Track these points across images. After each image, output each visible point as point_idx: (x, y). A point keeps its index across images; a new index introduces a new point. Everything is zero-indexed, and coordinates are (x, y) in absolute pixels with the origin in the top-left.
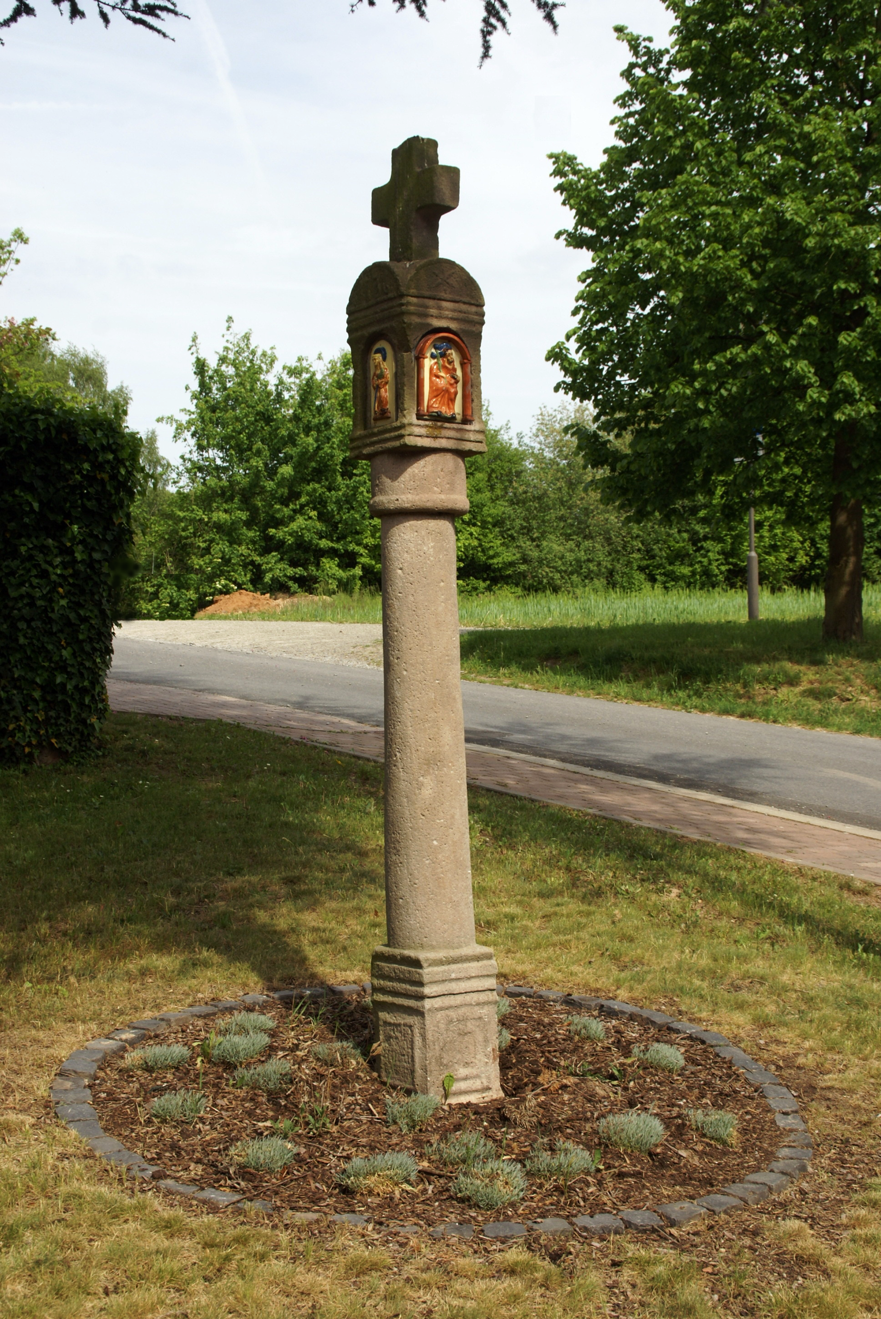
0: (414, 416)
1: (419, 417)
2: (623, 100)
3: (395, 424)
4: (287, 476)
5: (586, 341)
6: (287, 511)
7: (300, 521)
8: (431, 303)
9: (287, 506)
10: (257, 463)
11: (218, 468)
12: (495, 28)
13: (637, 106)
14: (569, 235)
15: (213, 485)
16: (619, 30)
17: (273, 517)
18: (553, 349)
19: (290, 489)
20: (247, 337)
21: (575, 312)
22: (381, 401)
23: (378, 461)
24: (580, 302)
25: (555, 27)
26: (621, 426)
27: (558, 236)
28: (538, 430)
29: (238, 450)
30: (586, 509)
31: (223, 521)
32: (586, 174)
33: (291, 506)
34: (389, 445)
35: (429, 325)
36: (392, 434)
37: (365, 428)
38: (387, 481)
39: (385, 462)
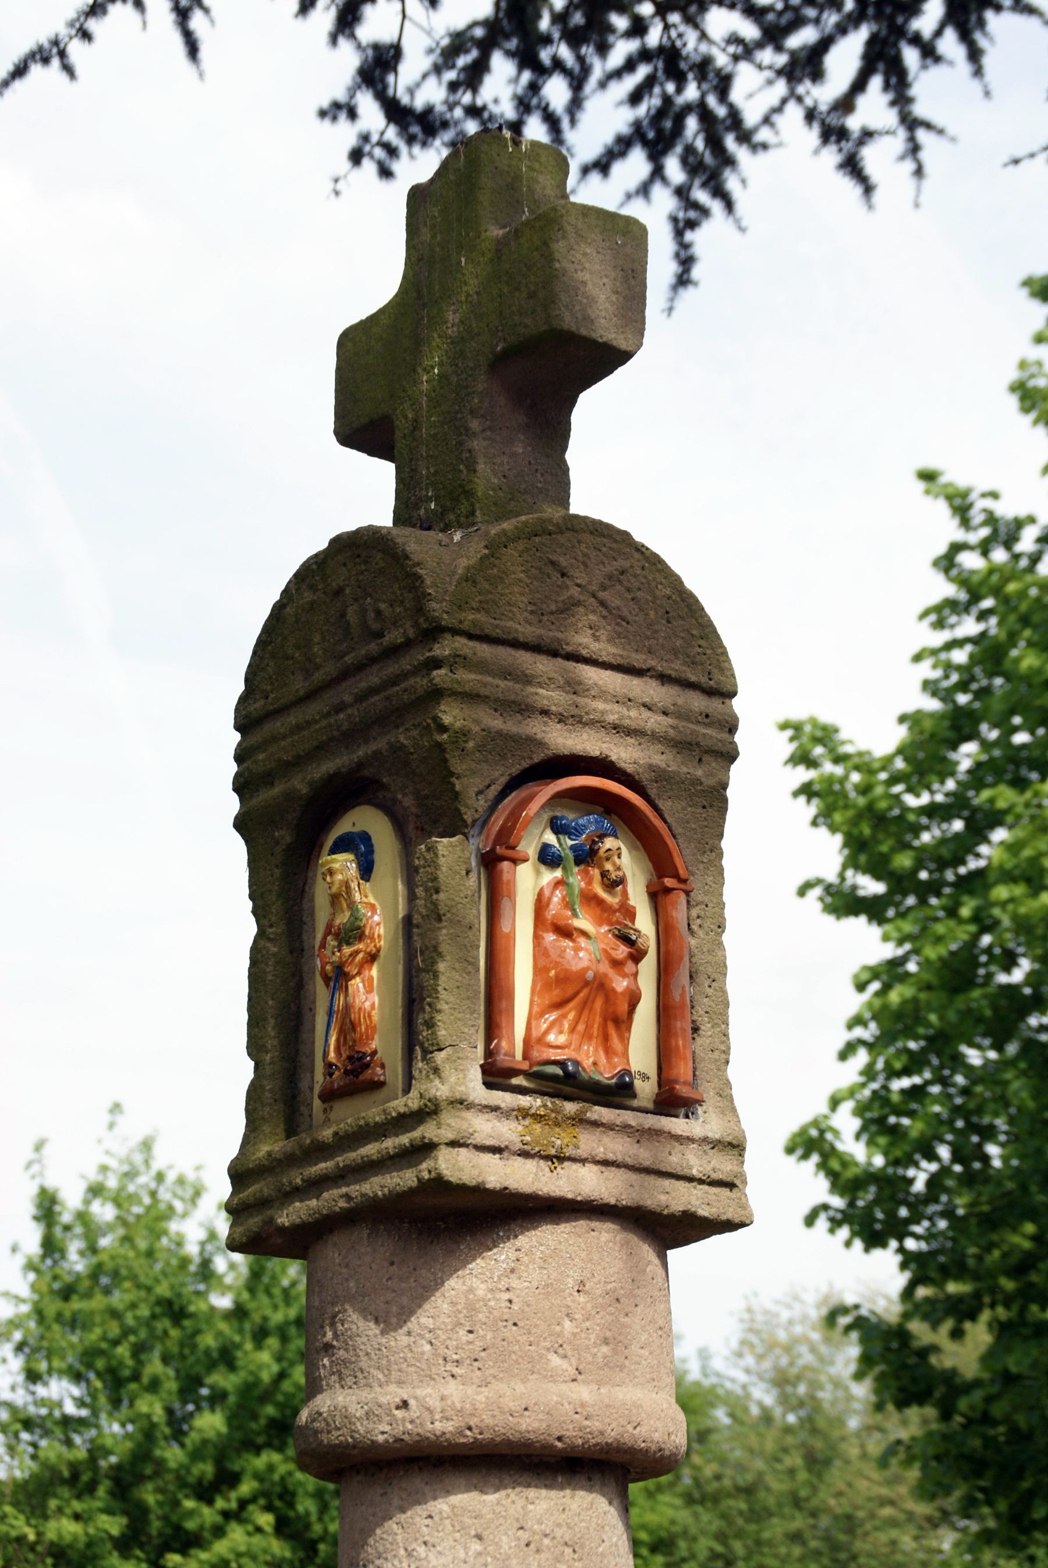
0: (475, 1075)
1: (495, 1075)
2: (941, 614)
3: (399, 1105)
4: (211, 1435)
5: (877, 1119)
6: (208, 1515)
7: (237, 1536)
8: (542, 665)
9: (210, 1502)
10: (152, 1407)
11: (66, 1421)
12: (705, 212)
13: (969, 627)
14: (829, 889)
15: (52, 1456)
16: (928, 476)
17: (178, 1528)
18: (803, 1131)
19: (220, 1461)
20: (147, 1146)
21: (846, 1053)
22: (348, 1025)
23: (331, 1252)
24: (859, 1032)
25: (868, 189)
26: (963, 1311)
27: (803, 890)
28: (743, 1342)
29: (113, 1381)
30: (849, 1517)
31: (68, 1538)
32: (864, 764)
33: (220, 1503)
34: (377, 1186)
35: (532, 742)
36: (390, 1144)
37: (291, 1131)
38: (362, 1329)
39: (359, 1256)
